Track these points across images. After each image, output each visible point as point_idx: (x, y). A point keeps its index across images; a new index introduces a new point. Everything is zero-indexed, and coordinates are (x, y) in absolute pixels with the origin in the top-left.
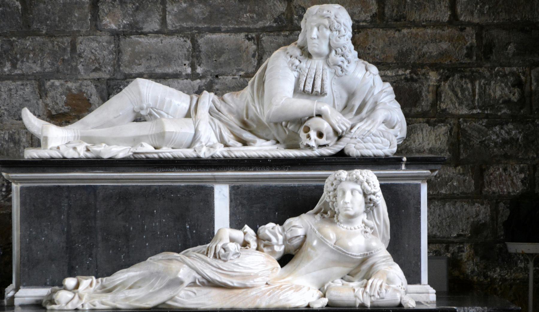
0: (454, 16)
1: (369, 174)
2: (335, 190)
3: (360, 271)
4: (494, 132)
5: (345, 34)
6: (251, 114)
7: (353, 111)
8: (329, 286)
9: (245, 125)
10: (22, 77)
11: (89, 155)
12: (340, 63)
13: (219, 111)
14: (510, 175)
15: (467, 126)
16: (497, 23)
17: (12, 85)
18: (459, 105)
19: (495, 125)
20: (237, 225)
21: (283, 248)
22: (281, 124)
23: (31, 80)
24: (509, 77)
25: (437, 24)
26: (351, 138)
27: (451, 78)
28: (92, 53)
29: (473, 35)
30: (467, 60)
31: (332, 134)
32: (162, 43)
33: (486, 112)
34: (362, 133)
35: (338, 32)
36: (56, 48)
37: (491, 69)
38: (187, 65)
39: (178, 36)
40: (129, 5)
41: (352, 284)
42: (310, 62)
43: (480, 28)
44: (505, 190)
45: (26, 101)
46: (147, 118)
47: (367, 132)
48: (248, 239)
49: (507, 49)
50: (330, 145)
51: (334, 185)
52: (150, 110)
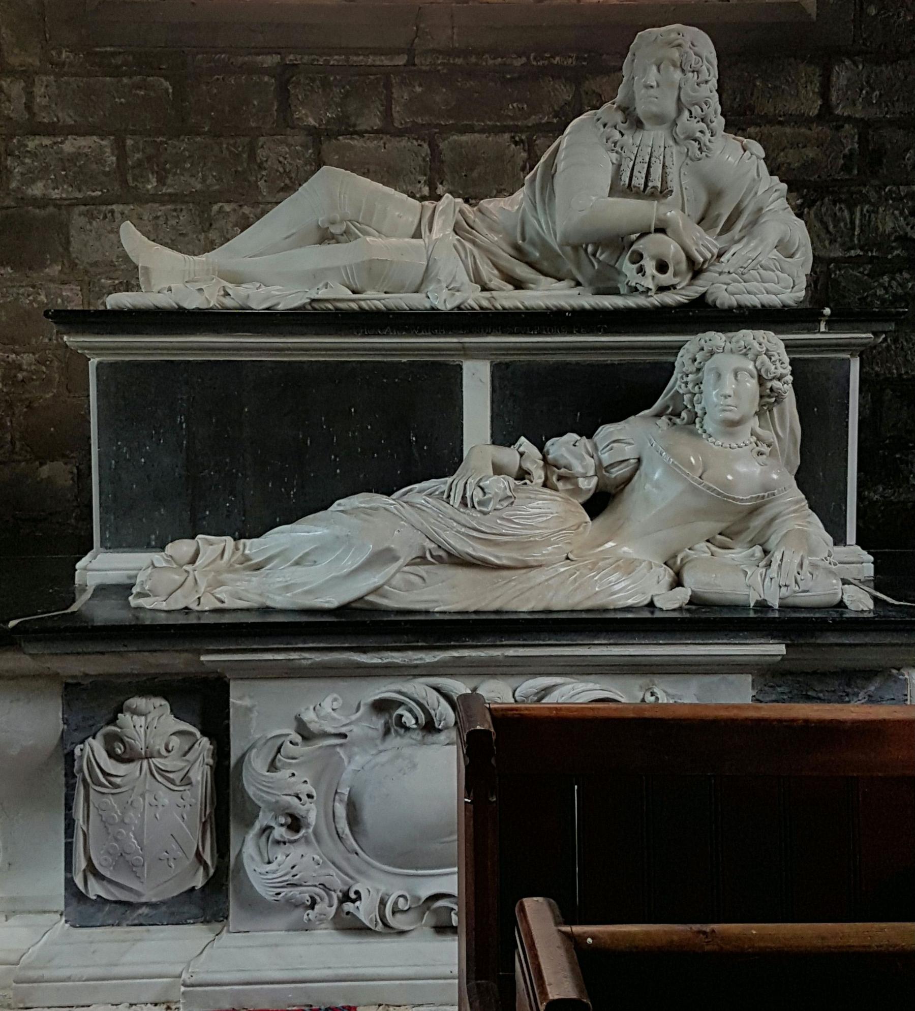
0: (826, 113)
1: (771, 340)
2: (699, 370)
3: (748, 528)
4: (882, 285)
5: (709, 78)
6: (529, 233)
7: (717, 227)
8: (687, 556)
9: (520, 254)
10: (173, 198)
11: (228, 302)
12: (698, 134)
13: (473, 228)
14: (902, 349)
15: (840, 275)
16: (890, 118)
17: (162, 210)
18: (830, 243)
19: (884, 275)
20: (505, 435)
21: (595, 480)
22: (586, 250)
23: (187, 202)
24: (905, 201)
25: (802, 120)
26: (720, 273)
27: (818, 203)
28: (280, 162)
29: (854, 137)
30: (843, 176)
31: (684, 266)
32: (385, 148)
33: (870, 254)
34: (741, 264)
35: (695, 73)
36: (226, 153)
37: (880, 188)
38: (422, 182)
39: (409, 138)
40: (334, 89)
41: (729, 555)
42: (639, 136)
43: (864, 125)
44: (895, 371)
45: (181, 234)
46: (340, 238)
47: (750, 261)
48: (528, 465)
49: (904, 159)
50: (678, 287)
51: (698, 361)
52: (348, 226)
